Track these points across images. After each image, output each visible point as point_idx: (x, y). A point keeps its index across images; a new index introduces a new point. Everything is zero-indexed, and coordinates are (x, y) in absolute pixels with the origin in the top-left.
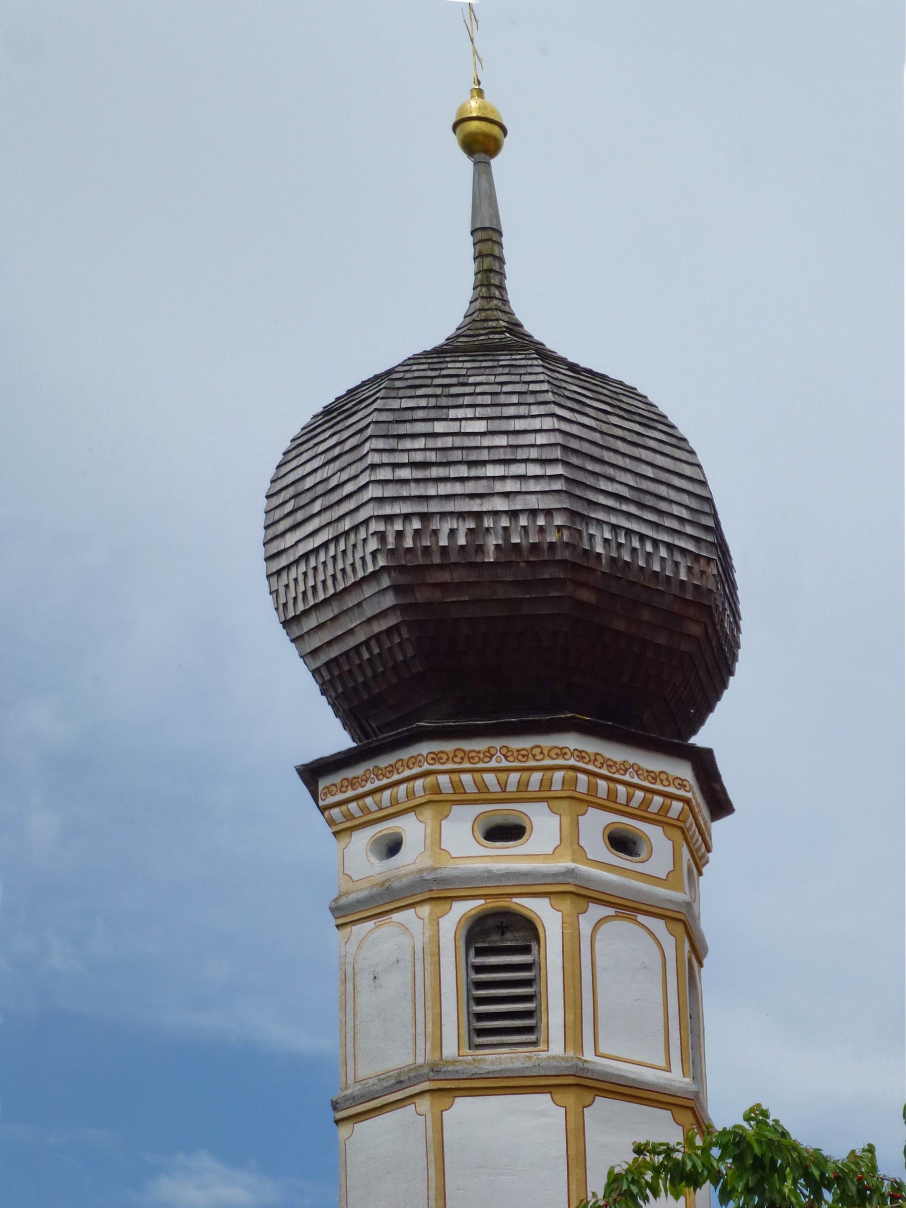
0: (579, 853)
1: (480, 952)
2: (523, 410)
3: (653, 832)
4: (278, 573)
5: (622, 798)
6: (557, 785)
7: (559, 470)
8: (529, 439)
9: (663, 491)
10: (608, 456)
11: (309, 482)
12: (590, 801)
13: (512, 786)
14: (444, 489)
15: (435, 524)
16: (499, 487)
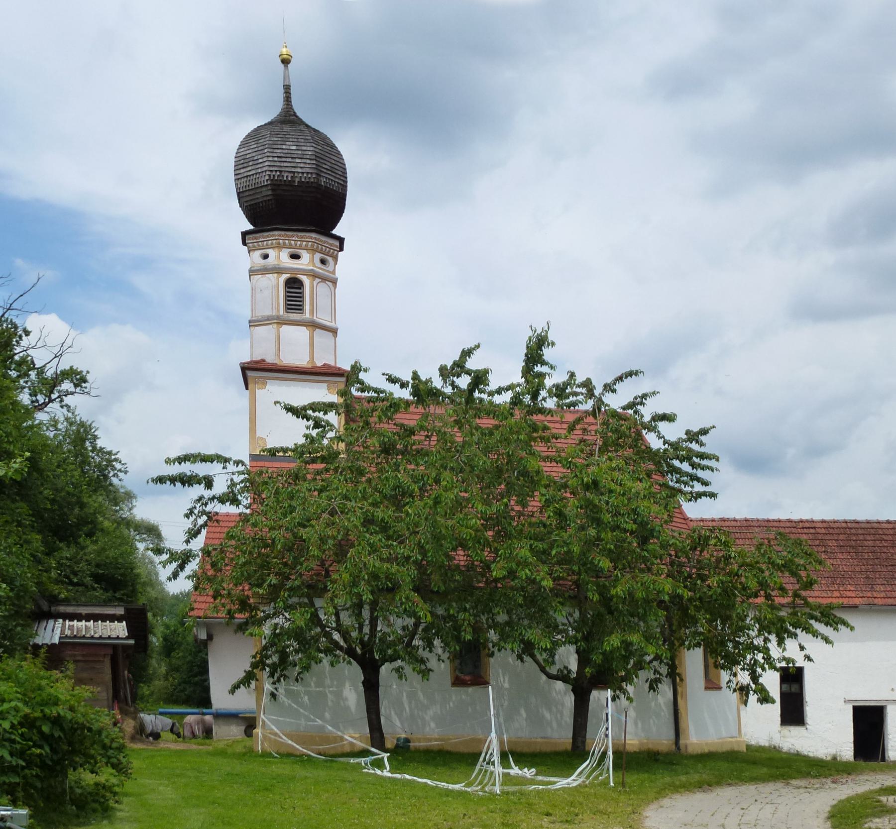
0: (314, 265)
1: (289, 288)
2: (305, 144)
4: (238, 179)
5: (315, 247)
6: (309, 246)
7: (314, 162)
8: (307, 152)
9: (336, 167)
10: (324, 158)
11: (248, 156)
13: (298, 245)
14: (286, 164)
15: (283, 174)
16: (299, 165)
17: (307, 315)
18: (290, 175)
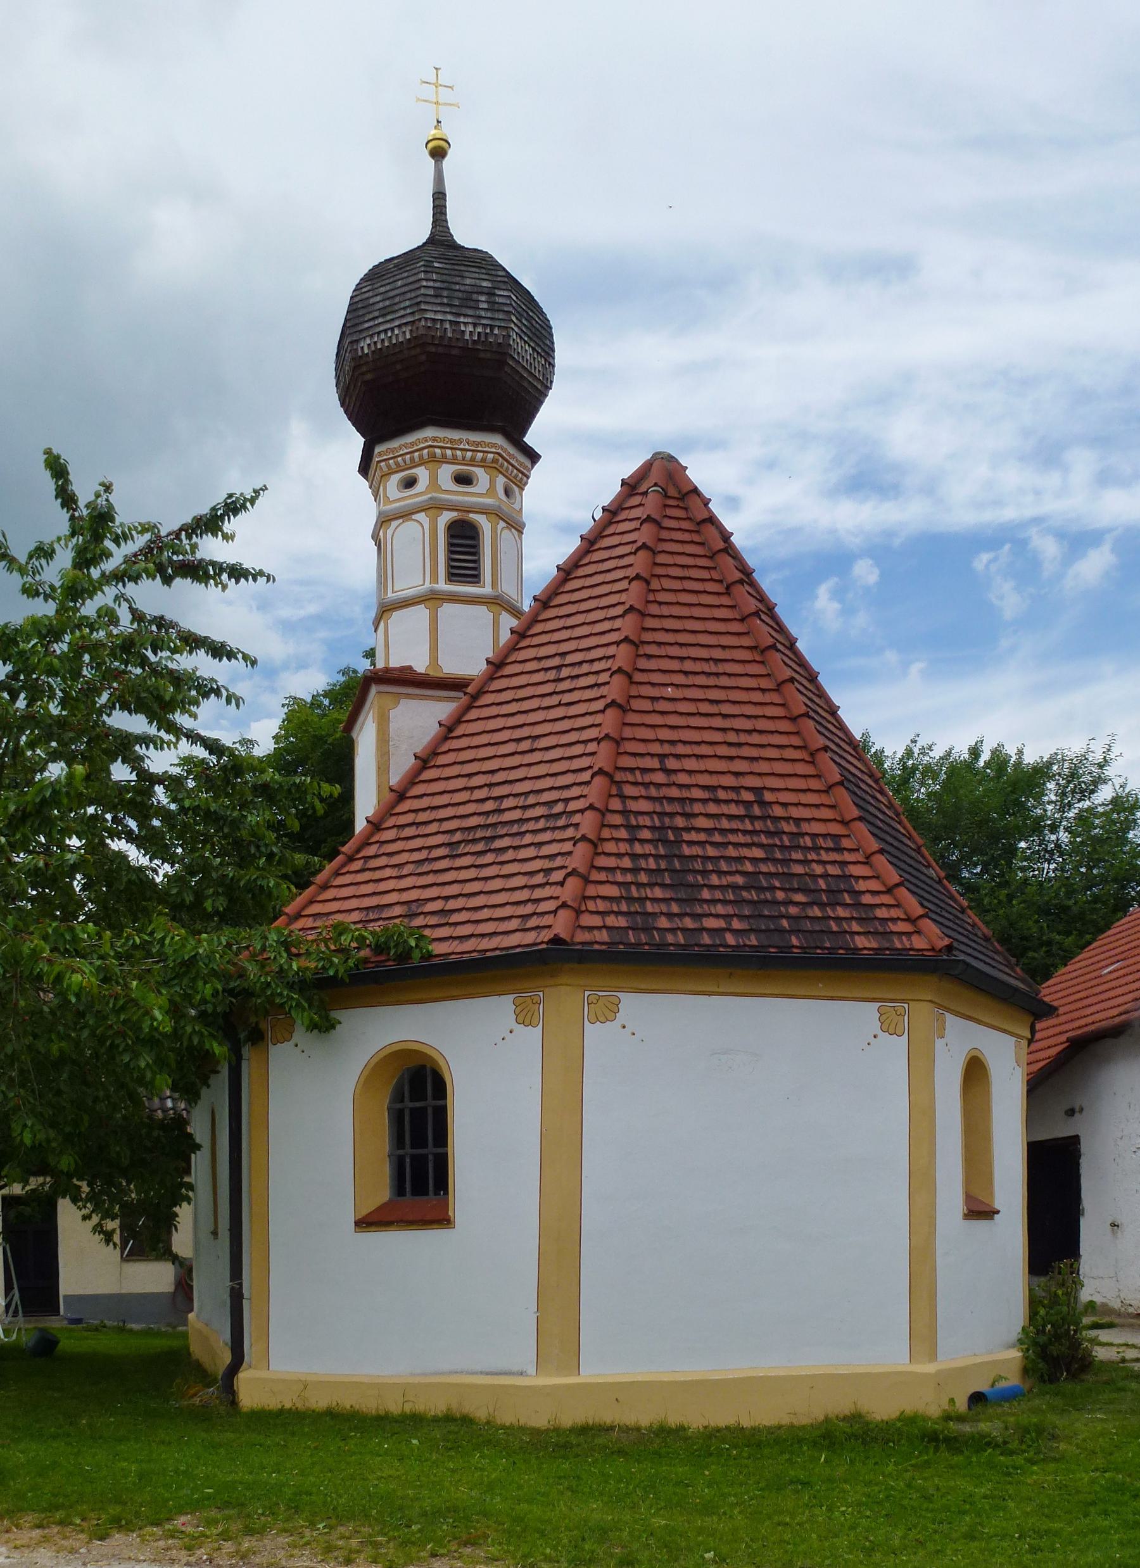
3: (479, 472)
12: (444, 460)
17: (486, 590)
18: (407, 329)
